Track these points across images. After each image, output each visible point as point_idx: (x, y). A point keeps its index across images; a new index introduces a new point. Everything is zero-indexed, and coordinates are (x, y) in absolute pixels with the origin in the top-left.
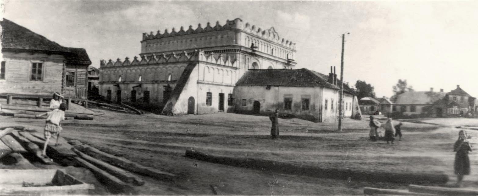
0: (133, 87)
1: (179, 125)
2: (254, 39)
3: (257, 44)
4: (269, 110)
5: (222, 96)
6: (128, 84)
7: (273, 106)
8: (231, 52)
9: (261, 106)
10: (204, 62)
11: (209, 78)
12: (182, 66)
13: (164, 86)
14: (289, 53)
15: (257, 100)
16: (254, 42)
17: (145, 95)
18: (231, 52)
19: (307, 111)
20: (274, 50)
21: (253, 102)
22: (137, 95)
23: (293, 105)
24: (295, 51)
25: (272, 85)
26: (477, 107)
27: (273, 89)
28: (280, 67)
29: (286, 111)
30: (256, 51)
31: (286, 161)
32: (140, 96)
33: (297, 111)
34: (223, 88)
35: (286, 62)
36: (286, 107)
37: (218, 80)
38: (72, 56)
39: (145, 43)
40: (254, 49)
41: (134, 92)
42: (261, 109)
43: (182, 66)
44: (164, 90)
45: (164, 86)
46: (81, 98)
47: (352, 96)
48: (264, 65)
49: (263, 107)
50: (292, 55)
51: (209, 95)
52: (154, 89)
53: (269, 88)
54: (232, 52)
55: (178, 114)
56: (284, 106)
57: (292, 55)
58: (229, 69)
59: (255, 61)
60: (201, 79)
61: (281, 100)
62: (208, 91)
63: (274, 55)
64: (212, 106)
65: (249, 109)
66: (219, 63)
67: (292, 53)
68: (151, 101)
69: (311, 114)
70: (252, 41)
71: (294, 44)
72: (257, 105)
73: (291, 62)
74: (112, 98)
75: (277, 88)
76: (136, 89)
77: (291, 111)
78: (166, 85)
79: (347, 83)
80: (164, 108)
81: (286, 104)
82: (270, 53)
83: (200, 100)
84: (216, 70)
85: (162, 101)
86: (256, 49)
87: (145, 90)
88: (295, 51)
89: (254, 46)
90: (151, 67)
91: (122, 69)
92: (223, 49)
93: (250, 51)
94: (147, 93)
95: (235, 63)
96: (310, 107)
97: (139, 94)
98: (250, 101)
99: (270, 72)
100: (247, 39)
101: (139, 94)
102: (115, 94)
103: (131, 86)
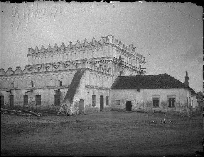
0: (26, 93)
2: (121, 52)
3: (123, 56)
4: (139, 108)
5: (102, 97)
6: (20, 90)
7: (143, 104)
8: (107, 62)
9: (132, 105)
11: (93, 83)
13: (55, 91)
15: (129, 100)
16: (121, 55)
17: (37, 99)
18: (107, 62)
19: (173, 108)
20: (133, 61)
21: (126, 102)
22: (29, 100)
23: (160, 103)
24: (145, 63)
25: (141, 88)
27: (142, 91)
28: (135, 74)
29: (154, 109)
30: (123, 61)
31: (67, 155)
32: (32, 100)
33: (164, 108)
34: (103, 91)
36: (154, 105)
37: (99, 85)
39: (31, 57)
41: (26, 97)
42: (133, 108)
44: (55, 94)
45: (55, 91)
46: (67, 98)
47: (15, 105)
48: (127, 73)
49: (134, 107)
51: (94, 96)
52: (45, 93)
53: (139, 91)
54: (101, 63)
55: (73, 115)
56: (153, 104)
59: (122, 70)
60: (88, 84)
61: (150, 99)
62: (93, 94)
64: (96, 107)
65: (122, 108)
66: (99, 71)
68: (42, 104)
69: (177, 110)
71: (144, 57)
72: (129, 105)
74: (4, 103)
75: (146, 90)
76: (27, 94)
77: (159, 108)
78: (57, 90)
80: (60, 110)
81: (170, 103)
83: (88, 102)
84: (98, 76)
85: (53, 103)
86: (123, 60)
87: (37, 94)
88: (145, 63)
90: (41, 75)
91: (14, 77)
92: (103, 60)
93: (119, 62)
94: (38, 97)
96: (175, 105)
97: (31, 98)
98: (123, 101)
99: (131, 78)
100: (117, 52)
101: (31, 98)
102: (8, 99)
103: (23, 92)
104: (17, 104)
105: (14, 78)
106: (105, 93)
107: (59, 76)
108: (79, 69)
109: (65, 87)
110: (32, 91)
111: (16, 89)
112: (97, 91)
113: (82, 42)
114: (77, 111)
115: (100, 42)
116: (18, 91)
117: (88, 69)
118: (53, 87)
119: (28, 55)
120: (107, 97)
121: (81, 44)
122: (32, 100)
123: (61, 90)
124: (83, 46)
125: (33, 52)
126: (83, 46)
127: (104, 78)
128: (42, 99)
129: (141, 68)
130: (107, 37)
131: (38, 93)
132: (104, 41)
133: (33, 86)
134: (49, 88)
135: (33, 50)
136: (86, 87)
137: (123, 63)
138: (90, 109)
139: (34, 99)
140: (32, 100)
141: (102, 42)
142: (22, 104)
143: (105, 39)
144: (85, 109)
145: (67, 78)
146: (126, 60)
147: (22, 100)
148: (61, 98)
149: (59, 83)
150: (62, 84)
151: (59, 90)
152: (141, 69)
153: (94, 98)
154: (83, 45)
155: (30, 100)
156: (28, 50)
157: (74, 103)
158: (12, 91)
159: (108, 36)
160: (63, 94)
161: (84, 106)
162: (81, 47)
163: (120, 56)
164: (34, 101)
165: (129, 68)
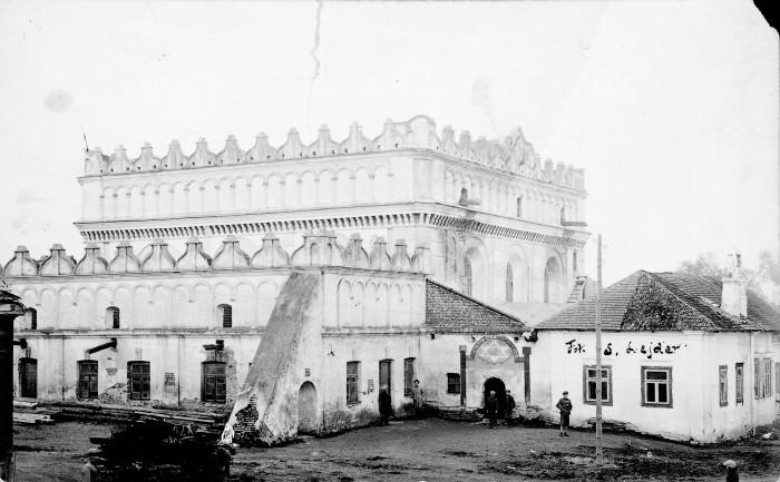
1: (31, 444)
5: (386, 364)
10: (337, 268)
12: (138, 287)
14: (567, 203)
16: (468, 187)
20: (523, 201)
26: (733, 476)
32: (111, 379)
34: (390, 341)
35: (560, 234)
38: (449, 313)
39: (95, 187)
40: (470, 208)
41: (88, 368)
43: (120, 287)
50: (577, 209)
57: (577, 209)
58: (403, 281)
63: (524, 217)
66: (375, 266)
67: (575, 202)
70: (464, 183)
71: (581, 171)
73: (573, 232)
79: (684, 264)
82: (512, 213)
85: (197, 395)
86: (476, 208)
89: (469, 197)
90: (151, 282)
93: (460, 215)
94: (139, 374)
95: (374, 263)
97: (111, 371)
101: (111, 371)
103: (78, 349)
104: (50, 392)
105: (39, 291)
106: (398, 351)
107: (226, 289)
108: (299, 268)
109: (242, 332)
110: (113, 344)
111: (47, 334)
112: (367, 343)
113: (308, 138)
114: (292, 427)
115: (380, 142)
116: (56, 343)
117: (330, 268)
118: (199, 332)
119: (81, 180)
120: (724, 404)
121: (307, 143)
122: (111, 379)
123: (228, 343)
124: (314, 153)
125: (105, 165)
126: (314, 153)
127: (395, 289)
128: (156, 378)
129: (567, 220)
130: (407, 124)
131: (138, 352)
132: (398, 140)
133: (116, 325)
134: (181, 333)
135: (105, 158)
136: (323, 336)
137: (477, 218)
138: (339, 415)
139: (122, 376)
140: (115, 380)
141: (387, 144)
142: (71, 394)
143: (402, 129)
144: (319, 414)
145: (256, 299)
146: (492, 204)
147: (73, 377)
148: (227, 371)
149: (221, 313)
150: (235, 323)
151: (220, 343)
152: (564, 223)
153: (355, 371)
154: (314, 149)
155: (104, 382)
156: (84, 155)
157: (280, 400)
158: (31, 343)
159: (411, 121)
160: (237, 357)
161: (314, 409)
162: (307, 157)
163: (464, 191)
164: (120, 386)
165: (507, 230)
